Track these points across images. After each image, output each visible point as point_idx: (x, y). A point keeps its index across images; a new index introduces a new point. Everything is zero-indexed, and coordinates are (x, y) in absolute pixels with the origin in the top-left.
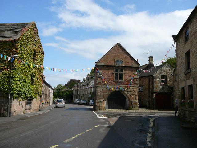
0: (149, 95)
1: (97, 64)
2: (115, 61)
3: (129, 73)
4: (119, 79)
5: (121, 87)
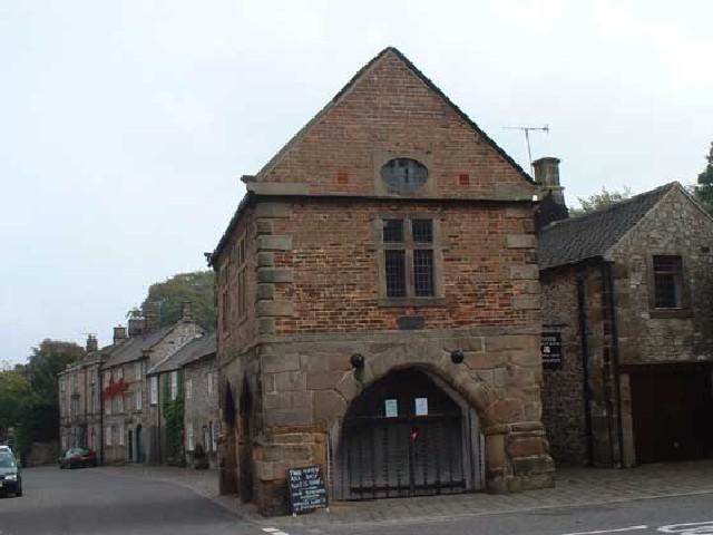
0: (586, 386)
1: (259, 189)
2: (379, 167)
3: (470, 225)
4: (410, 290)
5: (430, 346)
